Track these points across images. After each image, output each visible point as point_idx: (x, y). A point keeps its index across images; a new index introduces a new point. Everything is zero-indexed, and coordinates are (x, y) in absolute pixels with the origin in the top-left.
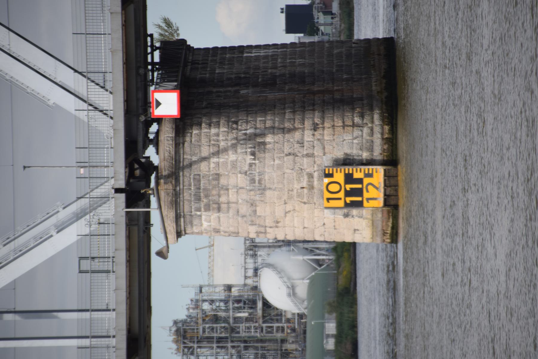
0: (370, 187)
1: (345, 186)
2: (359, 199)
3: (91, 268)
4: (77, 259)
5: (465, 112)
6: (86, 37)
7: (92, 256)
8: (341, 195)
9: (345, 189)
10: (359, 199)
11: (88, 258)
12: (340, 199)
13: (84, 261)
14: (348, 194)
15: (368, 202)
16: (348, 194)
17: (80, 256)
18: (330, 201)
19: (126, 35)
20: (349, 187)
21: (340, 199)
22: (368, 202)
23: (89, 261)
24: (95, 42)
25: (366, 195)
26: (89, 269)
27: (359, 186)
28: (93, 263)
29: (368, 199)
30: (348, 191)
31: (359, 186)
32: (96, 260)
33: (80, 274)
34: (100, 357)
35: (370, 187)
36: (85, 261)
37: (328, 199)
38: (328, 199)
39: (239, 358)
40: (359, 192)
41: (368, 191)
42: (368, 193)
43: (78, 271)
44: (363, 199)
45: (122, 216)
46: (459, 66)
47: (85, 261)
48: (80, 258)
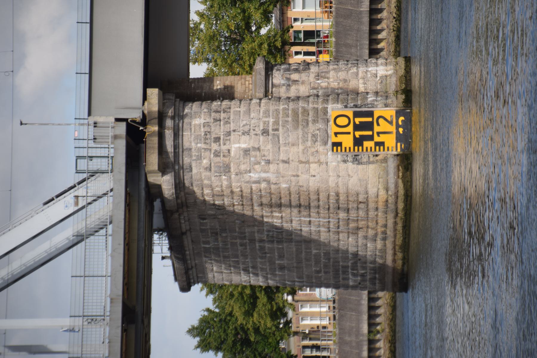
0: (381, 121)
1: (354, 120)
2: (370, 133)
3: (87, 168)
4: (75, 158)
5: (489, 112)
6: (88, 128)
7: (90, 155)
8: (350, 128)
9: (354, 123)
10: (370, 133)
11: (86, 157)
12: (349, 133)
13: (81, 160)
14: (357, 128)
15: (378, 136)
16: (357, 128)
17: (78, 155)
18: (338, 135)
19: (129, 255)
20: (358, 120)
21: (349, 133)
22: (378, 136)
23: (86, 160)
24: (95, 304)
25: (377, 129)
26: (86, 169)
27: (370, 119)
28: (90, 163)
29: (379, 134)
30: (358, 138)
31: (370, 119)
32: (95, 160)
33: (77, 174)
34: (93, 356)
35: (381, 121)
36: (83, 160)
37: (336, 134)
38: (336, 134)
39: (229, 356)
40: (369, 126)
41: (378, 124)
42: (379, 127)
43: (75, 171)
44: (373, 119)
45: (119, 244)
46: (484, 137)
47: (83, 160)
48: (77, 157)
